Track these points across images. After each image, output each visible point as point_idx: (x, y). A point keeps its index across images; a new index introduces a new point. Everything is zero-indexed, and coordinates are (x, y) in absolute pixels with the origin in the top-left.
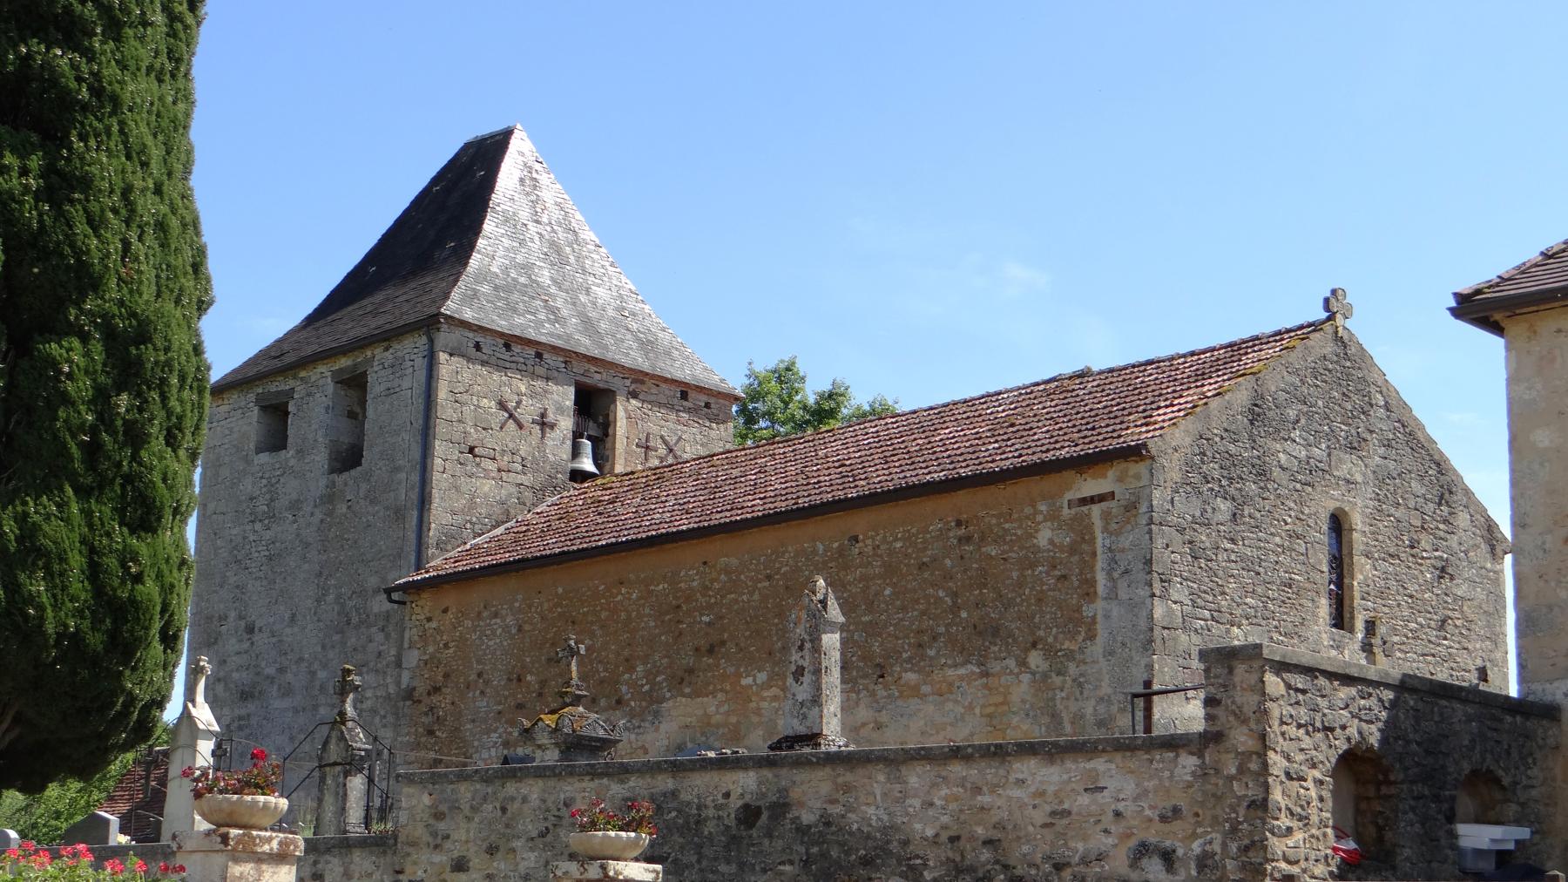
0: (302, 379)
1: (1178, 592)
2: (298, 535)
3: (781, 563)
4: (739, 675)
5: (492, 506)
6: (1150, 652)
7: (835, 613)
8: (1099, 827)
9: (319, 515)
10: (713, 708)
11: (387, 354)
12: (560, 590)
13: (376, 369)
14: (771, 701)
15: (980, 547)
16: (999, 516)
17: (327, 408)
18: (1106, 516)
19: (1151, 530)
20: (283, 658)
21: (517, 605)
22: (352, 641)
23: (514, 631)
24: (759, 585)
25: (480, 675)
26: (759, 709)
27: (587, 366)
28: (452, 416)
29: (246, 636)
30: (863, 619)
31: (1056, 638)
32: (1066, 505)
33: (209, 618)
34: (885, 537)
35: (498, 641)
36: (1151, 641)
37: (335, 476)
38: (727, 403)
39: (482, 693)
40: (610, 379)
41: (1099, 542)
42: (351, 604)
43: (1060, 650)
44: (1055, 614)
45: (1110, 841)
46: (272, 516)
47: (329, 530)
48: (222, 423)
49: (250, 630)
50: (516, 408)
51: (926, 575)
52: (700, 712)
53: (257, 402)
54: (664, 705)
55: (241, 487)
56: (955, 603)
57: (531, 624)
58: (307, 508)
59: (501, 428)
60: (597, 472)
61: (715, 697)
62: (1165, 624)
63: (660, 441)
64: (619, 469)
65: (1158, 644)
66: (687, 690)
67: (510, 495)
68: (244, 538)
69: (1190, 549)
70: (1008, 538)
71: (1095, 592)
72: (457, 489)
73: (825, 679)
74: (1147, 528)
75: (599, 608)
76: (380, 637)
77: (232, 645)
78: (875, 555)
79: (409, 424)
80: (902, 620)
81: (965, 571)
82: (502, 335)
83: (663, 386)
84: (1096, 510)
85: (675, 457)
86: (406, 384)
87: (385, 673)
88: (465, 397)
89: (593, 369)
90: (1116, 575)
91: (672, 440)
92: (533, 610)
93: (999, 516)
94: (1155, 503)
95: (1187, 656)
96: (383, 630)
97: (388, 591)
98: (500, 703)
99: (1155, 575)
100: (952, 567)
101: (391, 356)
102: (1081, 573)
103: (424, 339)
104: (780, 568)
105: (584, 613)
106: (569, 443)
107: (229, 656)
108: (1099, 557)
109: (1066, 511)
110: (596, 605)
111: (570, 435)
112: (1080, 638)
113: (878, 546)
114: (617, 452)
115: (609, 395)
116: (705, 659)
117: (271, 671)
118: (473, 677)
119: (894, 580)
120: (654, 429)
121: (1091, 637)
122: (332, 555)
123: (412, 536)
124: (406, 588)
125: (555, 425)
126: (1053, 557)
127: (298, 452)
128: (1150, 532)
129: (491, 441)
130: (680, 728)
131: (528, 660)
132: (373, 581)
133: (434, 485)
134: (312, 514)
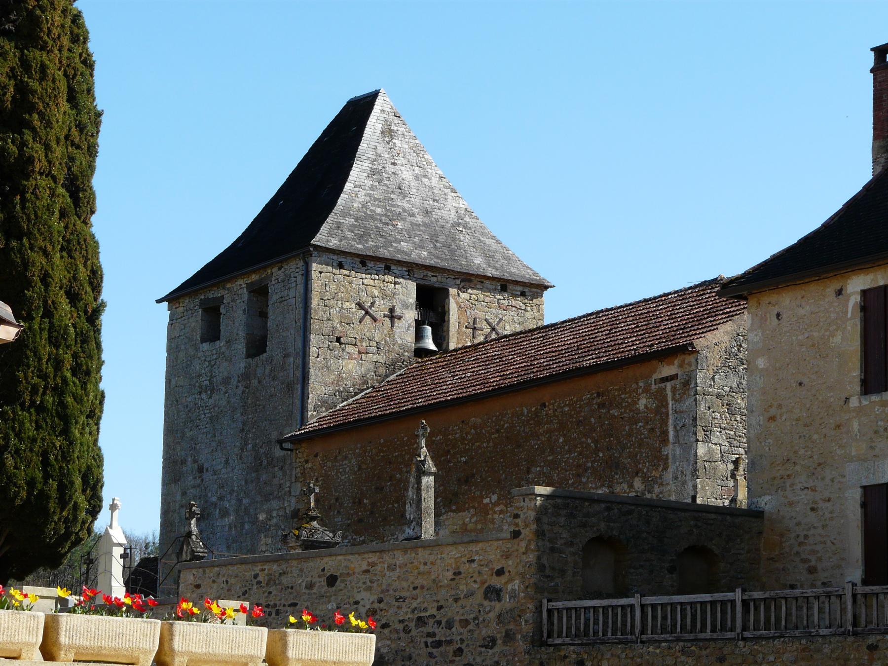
0: (228, 289)
1: (717, 437)
2: (228, 402)
3: (504, 421)
4: (482, 497)
5: (355, 378)
6: (695, 477)
7: (431, 466)
8: (473, 579)
9: (241, 388)
10: (468, 519)
11: (280, 272)
12: (382, 441)
13: (273, 283)
14: (500, 514)
15: (609, 410)
16: (619, 390)
17: (244, 311)
18: (674, 390)
19: (696, 398)
20: (222, 490)
21: (357, 451)
22: (264, 477)
23: (356, 469)
24: (493, 436)
25: (337, 500)
26: (493, 519)
27: (425, 272)
28: (323, 317)
29: (198, 475)
30: (548, 458)
31: (648, 469)
32: (653, 383)
33: (175, 462)
34: (559, 404)
35: (347, 476)
36: (696, 470)
37: (250, 359)
38: (538, 291)
39: (338, 512)
40: (444, 280)
41: (670, 405)
42: (262, 451)
43: (650, 477)
44: (648, 454)
45: (476, 586)
46: (213, 390)
47: (248, 399)
48: (178, 321)
49: (201, 470)
50: (371, 307)
51: (581, 428)
52: (460, 522)
53: (201, 306)
54: (441, 518)
55: (193, 367)
56: (596, 447)
57: (366, 464)
58: (234, 382)
59: (360, 322)
60: (436, 349)
61: (469, 512)
62: (706, 459)
63: (485, 323)
64: (452, 346)
65: (701, 472)
66: (454, 507)
67: (369, 370)
68: (195, 404)
69: (728, 409)
70: (624, 404)
71: (668, 439)
72: (328, 368)
73: (423, 504)
74: (694, 397)
75: (404, 453)
76: (279, 474)
77: (190, 481)
78: (555, 415)
79: (294, 322)
80: (568, 458)
81: (601, 426)
82: (358, 256)
83: (487, 282)
84: (669, 386)
85: (497, 334)
86: (292, 294)
87: (284, 499)
88: (332, 302)
89: (430, 274)
90: (678, 428)
91: (494, 322)
92: (367, 454)
93: (619, 390)
94: (698, 381)
95: (725, 479)
96: (282, 469)
97: (280, 442)
98: (349, 519)
99: (699, 428)
100: (595, 424)
101: (282, 274)
102: (661, 427)
103: (301, 263)
104: (504, 425)
105: (396, 456)
106: (413, 330)
107: (188, 488)
108: (670, 416)
109: (653, 387)
110: (403, 451)
111: (414, 324)
112: (660, 469)
113: (556, 410)
114: (451, 334)
115: (444, 293)
116: (463, 486)
117: (214, 499)
118: (333, 501)
119: (565, 432)
120: (480, 314)
121: (666, 468)
122: (250, 416)
123: (298, 403)
124: (293, 440)
125: (402, 317)
126: (647, 417)
127: (227, 342)
128: (695, 400)
129: (352, 332)
130: (450, 533)
131: (364, 489)
132: (275, 435)
133: (311, 367)
134: (237, 387)
